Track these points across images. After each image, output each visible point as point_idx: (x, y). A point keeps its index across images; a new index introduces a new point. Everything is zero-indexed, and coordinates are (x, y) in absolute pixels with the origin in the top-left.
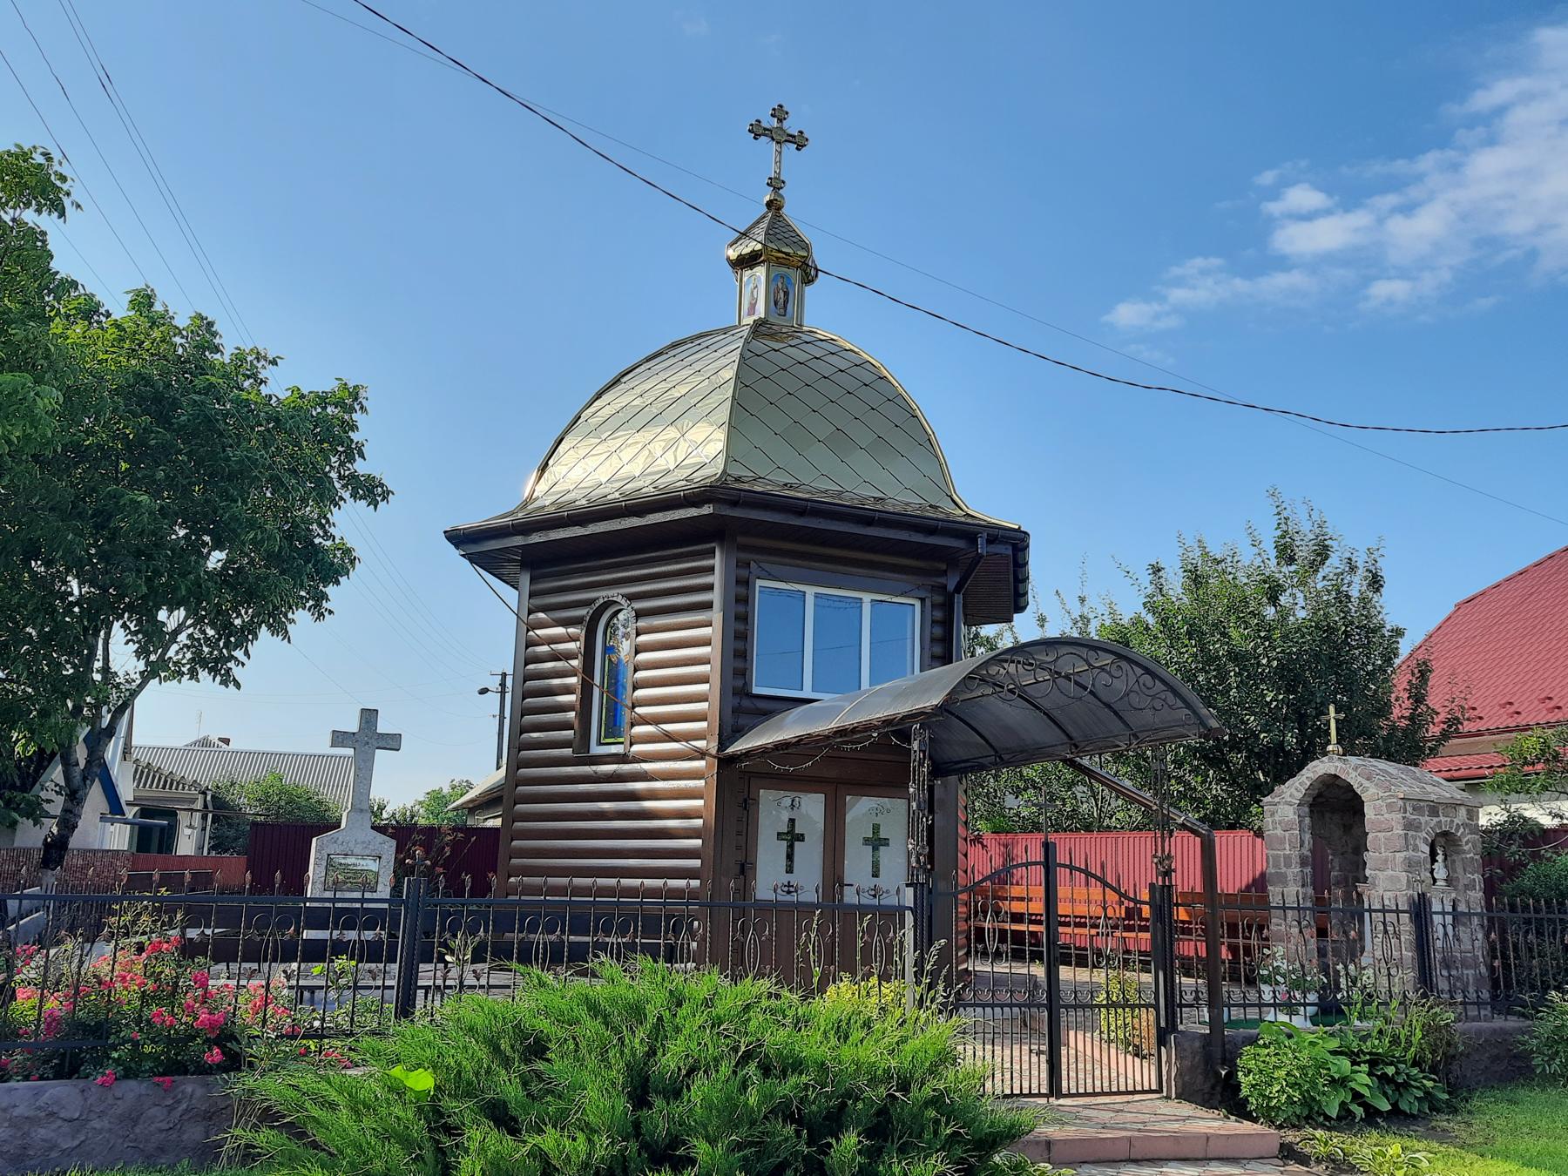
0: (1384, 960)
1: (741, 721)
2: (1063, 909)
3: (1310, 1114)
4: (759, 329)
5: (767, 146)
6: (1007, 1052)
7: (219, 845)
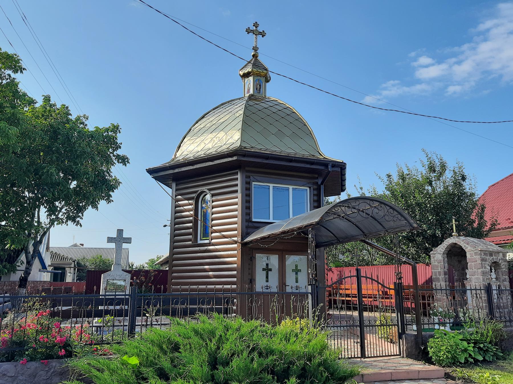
0: (475, 306)
1: (249, 230)
2: (364, 292)
3: (454, 362)
4: (251, 97)
5: (252, 36)
6: (346, 342)
7: (80, 279)
